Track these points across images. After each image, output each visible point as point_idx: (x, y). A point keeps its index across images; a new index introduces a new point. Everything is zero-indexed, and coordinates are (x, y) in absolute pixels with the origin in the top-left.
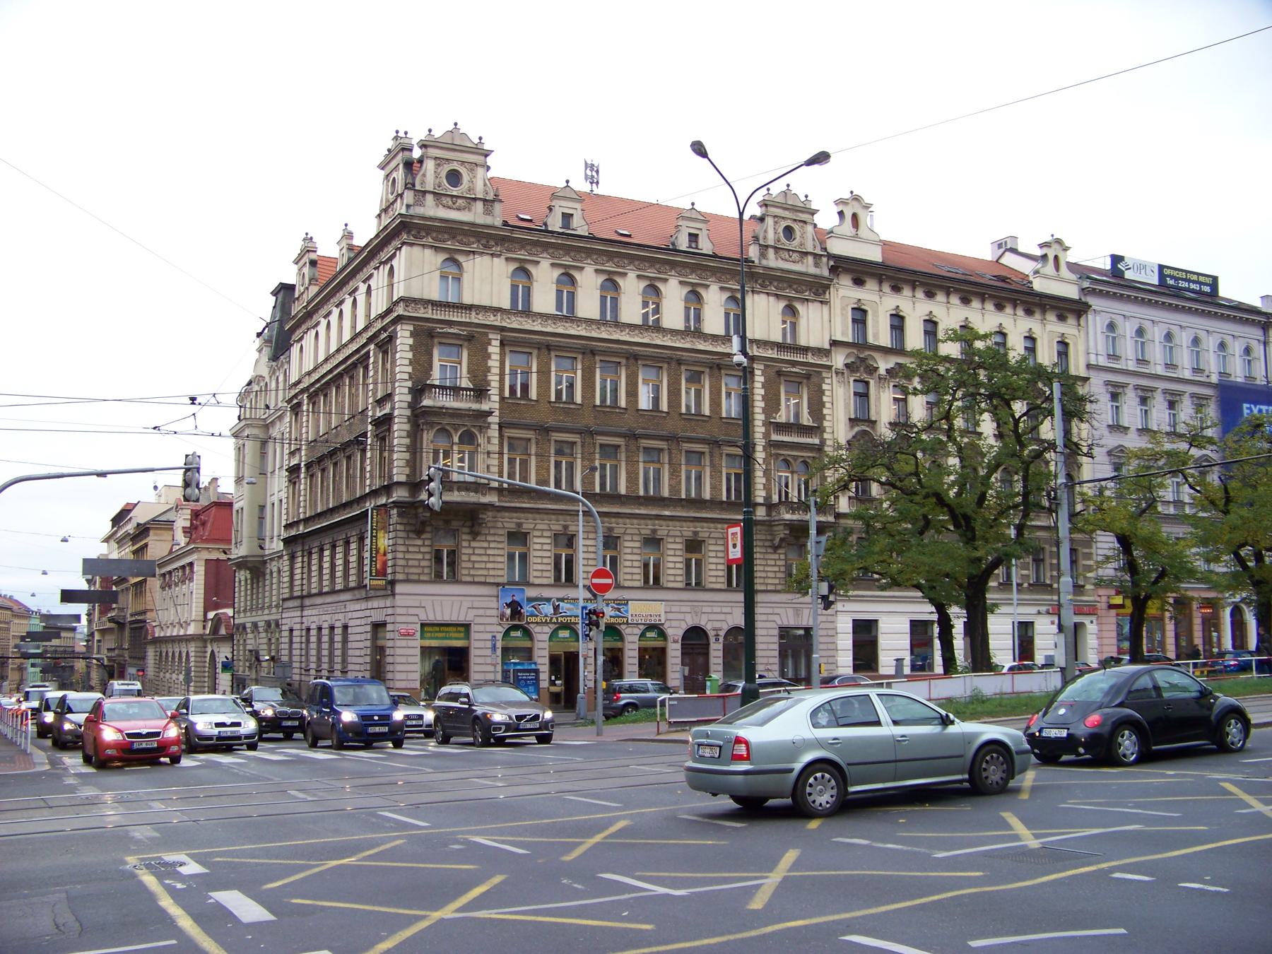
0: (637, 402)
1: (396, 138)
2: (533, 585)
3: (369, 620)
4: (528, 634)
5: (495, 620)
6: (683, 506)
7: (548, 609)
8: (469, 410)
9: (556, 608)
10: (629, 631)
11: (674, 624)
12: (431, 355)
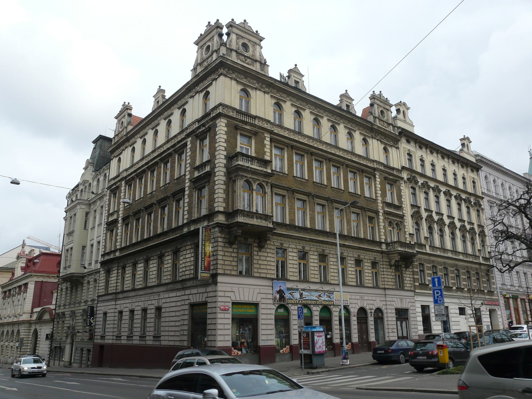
1: (123, 105)
2: (289, 280)
3: (187, 302)
4: (287, 309)
5: (271, 301)
6: (353, 241)
7: (297, 295)
8: (262, 171)
9: (301, 295)
11: (354, 306)
12: (236, 139)
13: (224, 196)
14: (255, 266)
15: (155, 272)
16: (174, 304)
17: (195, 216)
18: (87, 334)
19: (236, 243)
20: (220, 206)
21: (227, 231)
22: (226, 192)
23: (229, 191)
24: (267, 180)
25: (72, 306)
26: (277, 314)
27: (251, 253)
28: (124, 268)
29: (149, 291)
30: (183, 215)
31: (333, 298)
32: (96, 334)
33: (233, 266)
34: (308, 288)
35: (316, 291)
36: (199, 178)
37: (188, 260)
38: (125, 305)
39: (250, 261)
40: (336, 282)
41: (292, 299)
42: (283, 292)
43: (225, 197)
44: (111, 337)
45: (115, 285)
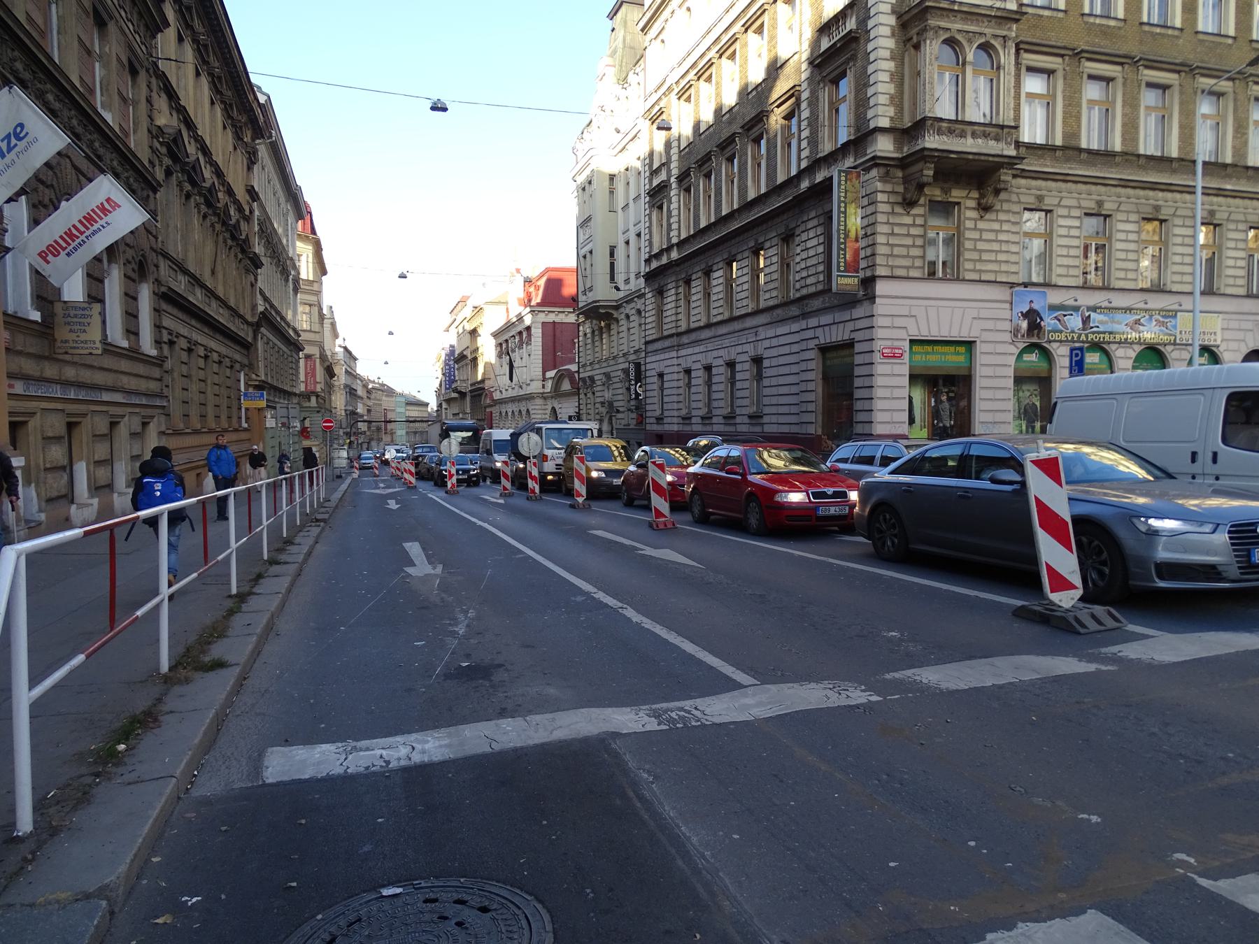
0: (1195, 21)
3: (812, 344)
4: (1046, 354)
5: (1007, 337)
7: (1075, 322)
9: (1086, 321)
10: (1175, 354)
13: (891, 88)
14: (967, 255)
15: (745, 287)
16: (786, 350)
17: (827, 148)
18: (634, 415)
19: (922, 201)
20: (882, 116)
21: (900, 174)
22: (898, 78)
23: (903, 76)
24: (1004, 33)
25: (604, 364)
26: (1023, 365)
27: (959, 226)
28: (688, 282)
29: (737, 326)
30: (800, 150)
31: (1175, 327)
32: (648, 414)
33: (914, 257)
34: (1105, 304)
35: (1129, 310)
36: (832, 53)
37: (812, 253)
38: (694, 358)
39: (955, 241)
40: (1187, 288)
41: (1061, 332)
42: (1039, 314)
43: (892, 91)
44: (675, 420)
45: (674, 311)
